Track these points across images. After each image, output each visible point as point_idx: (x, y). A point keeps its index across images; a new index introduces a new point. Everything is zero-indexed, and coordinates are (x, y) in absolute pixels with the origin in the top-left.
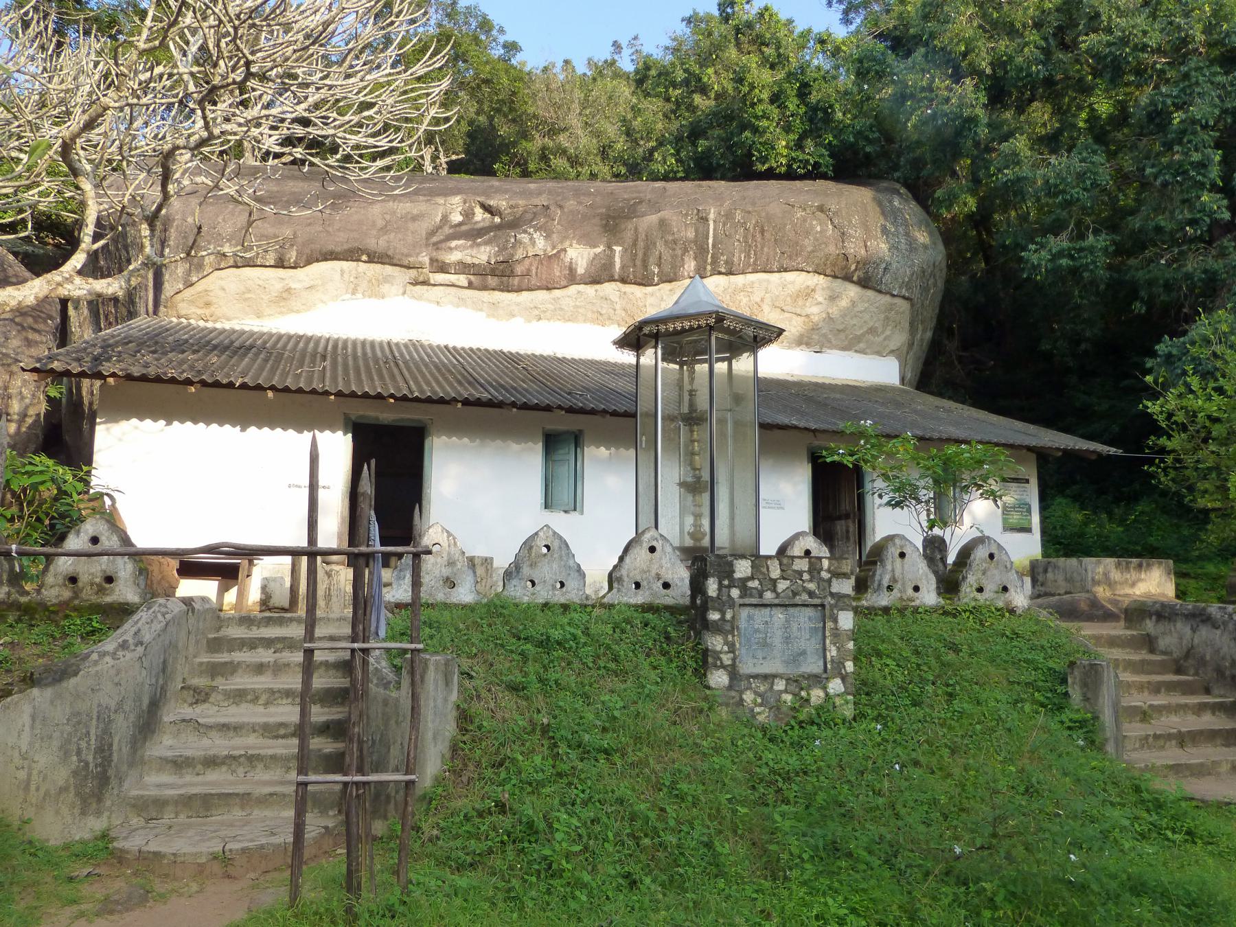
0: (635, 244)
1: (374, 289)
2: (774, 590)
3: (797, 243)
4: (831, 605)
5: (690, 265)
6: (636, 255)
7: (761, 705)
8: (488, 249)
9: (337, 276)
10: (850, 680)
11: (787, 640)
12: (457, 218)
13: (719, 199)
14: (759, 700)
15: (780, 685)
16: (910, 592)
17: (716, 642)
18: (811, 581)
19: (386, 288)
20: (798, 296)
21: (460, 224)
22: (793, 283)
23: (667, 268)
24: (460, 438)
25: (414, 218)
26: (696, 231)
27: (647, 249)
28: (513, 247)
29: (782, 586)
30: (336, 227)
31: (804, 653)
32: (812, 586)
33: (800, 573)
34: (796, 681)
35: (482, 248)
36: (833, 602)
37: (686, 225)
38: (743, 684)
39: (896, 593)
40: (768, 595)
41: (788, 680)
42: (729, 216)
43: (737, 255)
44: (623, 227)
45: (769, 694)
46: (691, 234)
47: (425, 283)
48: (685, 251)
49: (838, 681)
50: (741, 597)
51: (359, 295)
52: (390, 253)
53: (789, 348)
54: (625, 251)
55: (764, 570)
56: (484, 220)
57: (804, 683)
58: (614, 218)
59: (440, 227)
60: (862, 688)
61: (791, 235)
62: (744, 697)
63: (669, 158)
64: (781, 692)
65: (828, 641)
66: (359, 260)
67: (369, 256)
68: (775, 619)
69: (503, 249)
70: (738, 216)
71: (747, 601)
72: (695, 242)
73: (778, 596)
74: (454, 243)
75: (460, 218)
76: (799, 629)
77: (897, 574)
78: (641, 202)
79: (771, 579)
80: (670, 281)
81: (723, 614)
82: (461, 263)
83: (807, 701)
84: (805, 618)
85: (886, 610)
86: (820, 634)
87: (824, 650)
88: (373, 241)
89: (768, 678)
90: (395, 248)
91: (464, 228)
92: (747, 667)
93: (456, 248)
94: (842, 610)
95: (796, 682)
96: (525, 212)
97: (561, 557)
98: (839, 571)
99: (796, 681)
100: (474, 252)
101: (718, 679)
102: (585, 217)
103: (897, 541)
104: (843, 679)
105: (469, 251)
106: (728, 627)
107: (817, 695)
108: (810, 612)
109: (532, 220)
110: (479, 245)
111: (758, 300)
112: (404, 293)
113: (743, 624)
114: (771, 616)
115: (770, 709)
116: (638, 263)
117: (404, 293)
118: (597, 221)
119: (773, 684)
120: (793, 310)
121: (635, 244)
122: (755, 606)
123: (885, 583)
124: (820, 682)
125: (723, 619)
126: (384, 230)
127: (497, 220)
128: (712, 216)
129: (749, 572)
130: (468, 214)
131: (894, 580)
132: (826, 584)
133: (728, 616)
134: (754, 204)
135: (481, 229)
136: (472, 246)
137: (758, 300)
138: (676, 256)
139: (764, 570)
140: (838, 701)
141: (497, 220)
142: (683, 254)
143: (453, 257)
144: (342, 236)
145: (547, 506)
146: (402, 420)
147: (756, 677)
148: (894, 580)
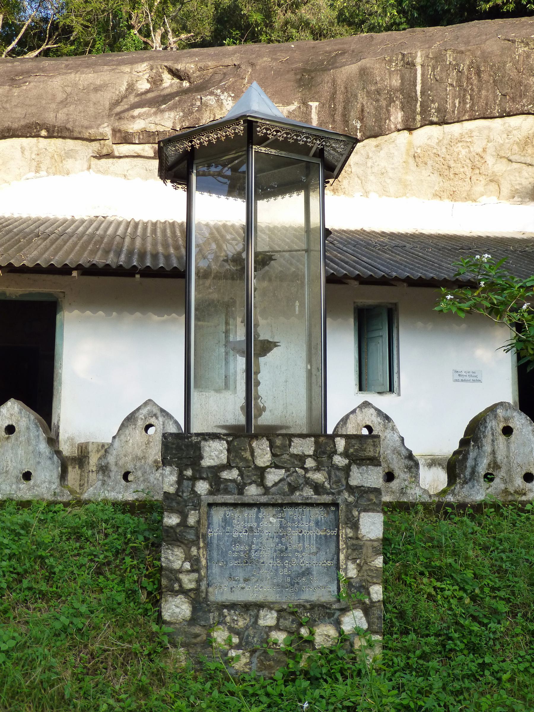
0: (333, 97)
1: (58, 167)
2: (261, 483)
3: (520, 83)
4: (348, 505)
5: (397, 116)
6: (335, 109)
7: (238, 647)
8: (172, 114)
9: (18, 154)
10: (377, 612)
11: (282, 554)
12: (144, 86)
13: (429, 41)
14: (235, 640)
15: (268, 619)
16: (519, 482)
17: (174, 557)
18: (317, 469)
19: (69, 164)
20: (526, 144)
21: (147, 92)
22: (519, 128)
23: (371, 122)
24: (169, 315)
25: (97, 89)
26: (402, 78)
27: (347, 103)
28: (200, 110)
29: (273, 477)
30: (13, 104)
31: (307, 572)
32: (319, 477)
33: (301, 459)
34: (293, 613)
35: (167, 114)
36: (351, 499)
37: (390, 73)
38: (213, 617)
39: (498, 484)
40: (253, 491)
41: (279, 611)
42: (439, 58)
43: (450, 101)
44: (319, 80)
45: (251, 632)
46: (396, 82)
47: (109, 155)
48: (391, 101)
49: (359, 613)
50: (210, 493)
51: (43, 173)
52: (69, 126)
53: (522, 203)
54: (322, 106)
55: (247, 455)
56: (171, 85)
57: (305, 616)
58: (309, 72)
59: (126, 97)
60: (394, 622)
61: (513, 74)
62: (215, 634)
63: (389, 9)
64: (270, 628)
65: (342, 557)
66: (38, 136)
67: (48, 131)
68: (264, 524)
69: (188, 114)
70: (450, 58)
71: (220, 498)
72: (401, 90)
73: (267, 490)
74: (136, 112)
75: (148, 86)
76: (301, 539)
77: (500, 457)
78: (343, 53)
79: (257, 468)
80: (375, 136)
81: (184, 517)
82: (144, 132)
83: (310, 642)
84: (309, 523)
85: (478, 508)
86: (333, 545)
87: (338, 568)
88: (52, 115)
89: (251, 608)
90: (74, 121)
91: (150, 95)
92: (221, 592)
93: (139, 116)
94: (366, 510)
95: (296, 616)
96: (215, 73)
97: (29, 440)
98: (361, 454)
99: (293, 613)
100: (158, 119)
101: (176, 609)
102: (278, 73)
103: (500, 412)
104: (367, 611)
105: (152, 119)
106: (191, 536)
107: (324, 634)
108: (317, 514)
109: (221, 81)
110: (163, 111)
111: (480, 150)
112: (89, 168)
113: (215, 532)
114: (258, 520)
115: (253, 652)
116: (338, 118)
117: (89, 168)
118: (291, 76)
119: (257, 617)
120: (522, 159)
121: (333, 97)
122: (235, 505)
123: (482, 469)
124: (330, 615)
125: (183, 523)
126: (64, 103)
127: (186, 84)
128: (419, 60)
129: (223, 458)
130: (156, 81)
131: (495, 465)
132: (341, 474)
133: (192, 520)
134: (467, 43)
135: (168, 95)
136: (155, 114)
137: (480, 150)
138: (381, 107)
139: (247, 455)
140: (359, 643)
141: (186, 84)
142: (388, 105)
143: (136, 126)
144: (20, 112)
145: (361, 389)
146: (30, 294)
147: (232, 606)
148: (495, 465)
